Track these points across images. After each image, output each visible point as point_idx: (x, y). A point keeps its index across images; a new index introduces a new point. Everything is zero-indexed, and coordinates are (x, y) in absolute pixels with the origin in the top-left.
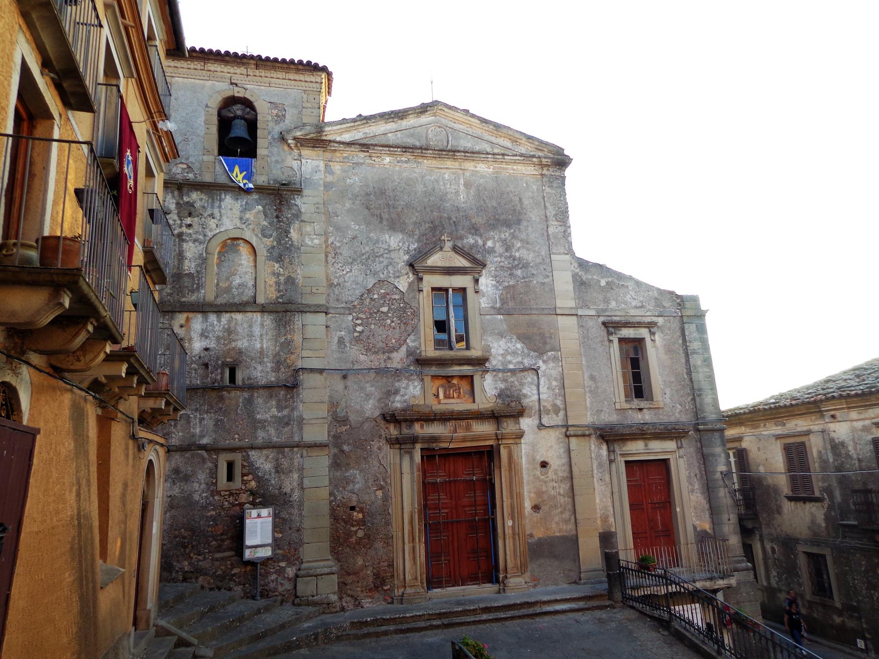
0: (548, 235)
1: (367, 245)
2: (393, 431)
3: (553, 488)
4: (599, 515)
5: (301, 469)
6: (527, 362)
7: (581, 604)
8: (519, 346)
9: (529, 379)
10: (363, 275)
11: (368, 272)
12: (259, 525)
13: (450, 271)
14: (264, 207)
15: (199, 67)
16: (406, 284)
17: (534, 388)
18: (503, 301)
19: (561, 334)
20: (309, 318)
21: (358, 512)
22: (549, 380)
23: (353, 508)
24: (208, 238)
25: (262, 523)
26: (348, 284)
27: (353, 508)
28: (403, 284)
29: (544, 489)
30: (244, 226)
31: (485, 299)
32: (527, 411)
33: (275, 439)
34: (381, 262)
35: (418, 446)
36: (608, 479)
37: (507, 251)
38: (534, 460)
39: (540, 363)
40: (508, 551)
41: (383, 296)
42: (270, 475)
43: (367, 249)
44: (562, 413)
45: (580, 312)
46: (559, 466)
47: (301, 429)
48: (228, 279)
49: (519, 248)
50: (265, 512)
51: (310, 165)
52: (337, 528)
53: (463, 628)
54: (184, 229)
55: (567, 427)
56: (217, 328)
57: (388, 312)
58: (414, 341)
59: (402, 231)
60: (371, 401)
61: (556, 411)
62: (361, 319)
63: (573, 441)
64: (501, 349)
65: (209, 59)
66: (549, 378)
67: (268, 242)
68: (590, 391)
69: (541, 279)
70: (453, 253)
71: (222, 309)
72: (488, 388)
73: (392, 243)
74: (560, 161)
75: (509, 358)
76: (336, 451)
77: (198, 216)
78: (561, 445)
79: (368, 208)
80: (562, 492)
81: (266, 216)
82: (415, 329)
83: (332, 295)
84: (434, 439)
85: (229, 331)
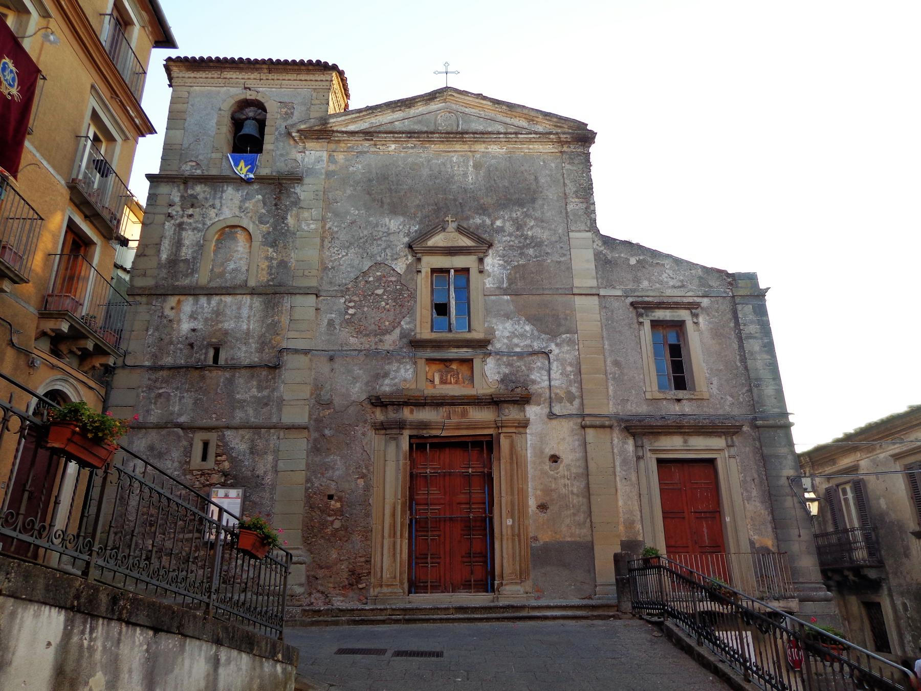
0: (567, 213)
1: (366, 228)
2: (379, 415)
3: (565, 485)
4: (622, 520)
5: (276, 452)
6: (536, 346)
8: (528, 328)
9: (539, 364)
11: (365, 255)
13: (451, 251)
14: (264, 197)
15: (216, 75)
16: (404, 266)
18: (511, 281)
20: (299, 300)
21: (337, 501)
22: (562, 364)
26: (343, 267)
27: (331, 497)
28: (400, 266)
30: (242, 215)
31: (490, 279)
32: (533, 398)
33: (253, 420)
35: (407, 433)
37: (518, 229)
38: (542, 452)
39: (553, 346)
40: (505, 554)
41: (379, 279)
43: (366, 232)
44: (577, 402)
45: (602, 292)
47: (280, 410)
51: (314, 156)
54: (185, 219)
55: (583, 416)
56: (206, 310)
57: (383, 294)
58: (409, 323)
59: (404, 214)
60: (358, 385)
61: (571, 398)
62: (354, 301)
63: (590, 433)
64: (507, 332)
65: (225, 68)
66: (563, 363)
67: (264, 228)
68: (614, 379)
69: (556, 258)
70: (457, 234)
72: (490, 374)
74: (582, 137)
75: (516, 341)
78: (576, 437)
80: (575, 490)
81: (265, 204)
82: (411, 311)
84: (425, 425)
85: (218, 313)
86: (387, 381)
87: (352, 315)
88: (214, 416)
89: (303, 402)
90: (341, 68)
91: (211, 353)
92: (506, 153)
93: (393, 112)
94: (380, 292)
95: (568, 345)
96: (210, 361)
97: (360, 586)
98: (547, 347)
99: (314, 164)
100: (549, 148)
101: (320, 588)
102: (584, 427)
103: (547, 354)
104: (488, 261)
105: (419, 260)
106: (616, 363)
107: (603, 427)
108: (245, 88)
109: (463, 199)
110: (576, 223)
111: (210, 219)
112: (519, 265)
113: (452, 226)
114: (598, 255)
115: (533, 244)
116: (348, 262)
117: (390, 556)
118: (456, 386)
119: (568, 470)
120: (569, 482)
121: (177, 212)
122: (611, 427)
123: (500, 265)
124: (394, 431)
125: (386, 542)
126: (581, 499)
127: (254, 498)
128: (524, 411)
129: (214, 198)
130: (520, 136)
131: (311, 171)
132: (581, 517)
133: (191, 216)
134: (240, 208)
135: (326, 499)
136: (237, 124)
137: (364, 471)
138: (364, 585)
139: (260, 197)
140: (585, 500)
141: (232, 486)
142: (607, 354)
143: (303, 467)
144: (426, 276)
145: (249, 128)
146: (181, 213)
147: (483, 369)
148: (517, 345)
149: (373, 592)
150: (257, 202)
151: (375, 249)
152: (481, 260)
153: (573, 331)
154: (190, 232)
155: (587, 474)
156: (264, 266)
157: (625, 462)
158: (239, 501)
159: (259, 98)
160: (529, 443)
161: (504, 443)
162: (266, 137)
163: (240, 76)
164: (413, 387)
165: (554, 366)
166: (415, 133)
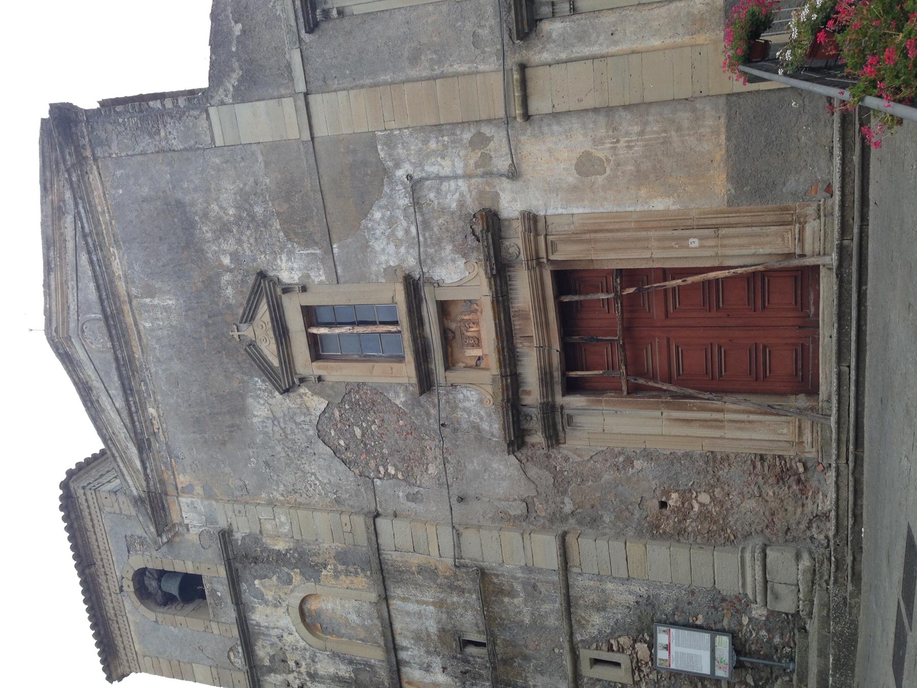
0: (185, 149)
1: (273, 448)
2: (537, 438)
3: (629, 147)
4: (687, 39)
5: (599, 577)
6: (404, 201)
7: (799, 284)
8: (377, 215)
9: (432, 195)
10: (315, 457)
11: (309, 450)
12: (680, 649)
13: (281, 332)
14: (255, 578)
15: (115, 625)
16: (316, 398)
17: (445, 186)
18: (308, 241)
19: (346, 131)
20: (385, 540)
21: (669, 497)
22: (428, 156)
23: (663, 505)
24: (307, 646)
25: (677, 645)
26: (332, 479)
27: (663, 505)
28: (318, 404)
29: (630, 168)
30: (284, 604)
31: (312, 274)
32: (487, 205)
33: (557, 605)
34: (293, 432)
35: (560, 399)
36: (611, 18)
37: (231, 231)
38: (574, 189)
39: (400, 173)
40: (750, 248)
41: (341, 433)
42: (609, 618)
43: (279, 449)
44: (487, 130)
45: (301, 87)
46: (585, 135)
47: (540, 571)
48: (353, 628)
49: (221, 207)
50: (662, 638)
51: (191, 512)
52: (693, 531)
53: (866, 421)
54: (303, 669)
55: (508, 120)
56: (416, 652)
57: (361, 427)
58: (397, 393)
59: (243, 397)
60: (495, 466)
61: (479, 141)
62: (377, 466)
63: (538, 105)
64: (389, 250)
65: (103, 616)
66: (424, 157)
67: (297, 578)
68: (440, 62)
69: (259, 167)
70: (255, 323)
71: (391, 645)
72: (459, 275)
73: (264, 414)
74: (66, 130)
75: (400, 234)
76: (572, 521)
77: (284, 653)
78: (546, 129)
79: (224, 443)
80: (636, 129)
81: (265, 577)
82: (378, 390)
83: (351, 503)
84: (546, 379)
85: (418, 638)
86: (485, 426)
87: (397, 469)
88: (557, 651)
89: (527, 542)
90: (63, 477)
91: (471, 650)
92: (119, 247)
93: (103, 410)
94: (358, 432)
95: (395, 147)
96: (482, 651)
97: (801, 470)
98: (403, 183)
99: (200, 514)
100: (94, 177)
101: (802, 527)
102: (527, 117)
103: (415, 185)
104: (286, 277)
105: (302, 380)
106: (414, 59)
107: (524, 83)
108: (121, 590)
109: (202, 313)
110: (198, 135)
111: (298, 642)
112: (283, 229)
113: (247, 331)
114: (242, 95)
115: (247, 206)
116: (323, 471)
117: (750, 429)
118: (482, 323)
119: (601, 142)
120: (622, 140)
121: (295, 678)
122: (523, 68)
123: (289, 259)
124: (559, 419)
125: (729, 434)
126: (651, 118)
127: (669, 608)
128: (510, 220)
129: (270, 635)
130: (87, 230)
131: (210, 520)
132: (684, 117)
133: (297, 664)
134: (276, 606)
135: (667, 512)
136: (168, 600)
137: (621, 459)
138: (800, 465)
139: (257, 582)
140: (653, 110)
141: (653, 636)
142: (402, 76)
143: (618, 545)
144: (326, 368)
145: (173, 588)
146: (295, 674)
147: (450, 286)
148: (407, 232)
149: (811, 453)
150: (264, 587)
151: (300, 438)
152: (287, 290)
153: (371, 142)
154: (318, 666)
155: (608, 110)
156: (348, 582)
157: (582, 37)
158: (673, 630)
159: (130, 575)
160: (560, 211)
161: (565, 253)
162: (178, 569)
163: (109, 598)
164: (490, 389)
165: (431, 169)
166: (123, 385)
